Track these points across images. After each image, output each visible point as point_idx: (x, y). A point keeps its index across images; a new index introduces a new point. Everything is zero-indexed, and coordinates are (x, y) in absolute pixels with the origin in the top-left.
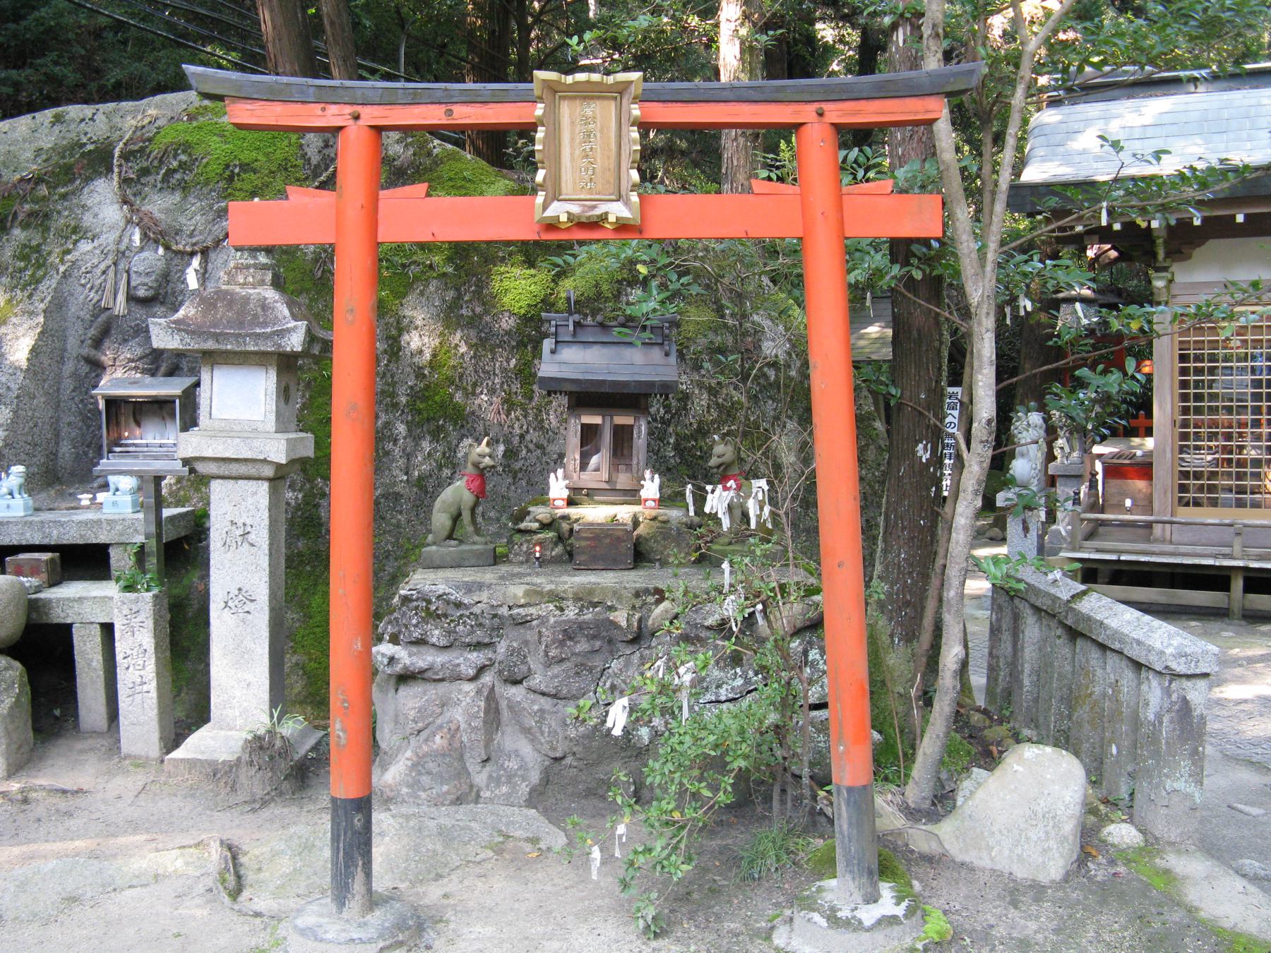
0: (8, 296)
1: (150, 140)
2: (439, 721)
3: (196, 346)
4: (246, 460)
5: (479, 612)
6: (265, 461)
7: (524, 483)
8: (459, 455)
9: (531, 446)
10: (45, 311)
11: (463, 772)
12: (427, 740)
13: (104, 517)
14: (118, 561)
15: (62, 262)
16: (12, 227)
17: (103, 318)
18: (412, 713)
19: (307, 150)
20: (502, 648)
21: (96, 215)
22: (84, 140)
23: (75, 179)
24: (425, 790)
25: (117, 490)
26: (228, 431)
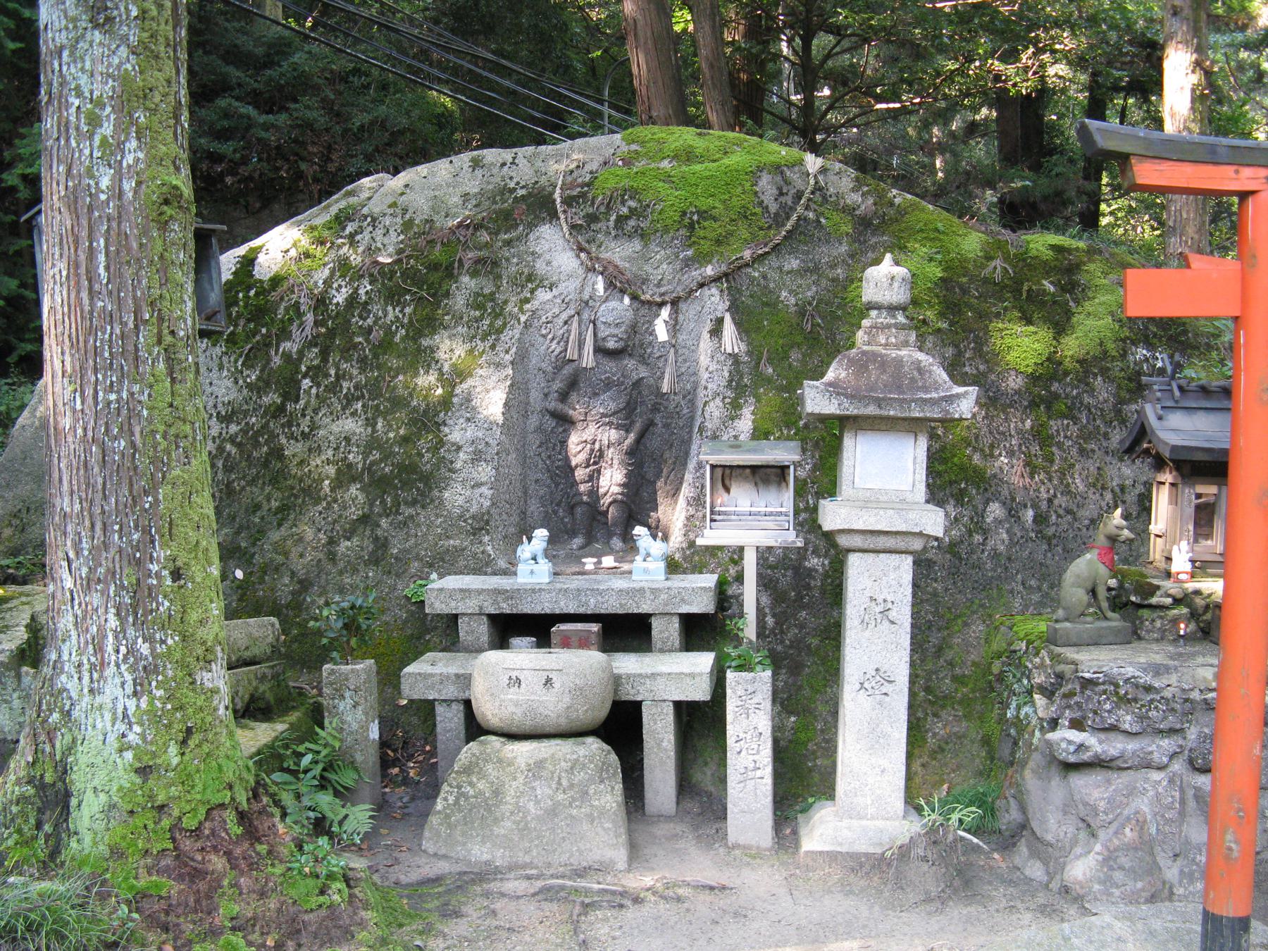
0: (468, 346)
1: (588, 185)
2: (1126, 812)
3: (856, 412)
4: (897, 533)
5: (1170, 696)
6: (920, 534)
7: (1059, 549)
8: (988, 520)
9: (1061, 512)
10: (512, 363)
11: (1153, 869)
12: (1116, 833)
13: (635, 585)
14: (661, 632)
15: (521, 310)
16: (459, 274)
17: (568, 370)
18: (1102, 803)
19: (763, 197)
20: (1192, 733)
21: (549, 263)
22: (512, 185)
23: (517, 225)
24: (1118, 887)
25: (648, 555)
26: (868, 502)
